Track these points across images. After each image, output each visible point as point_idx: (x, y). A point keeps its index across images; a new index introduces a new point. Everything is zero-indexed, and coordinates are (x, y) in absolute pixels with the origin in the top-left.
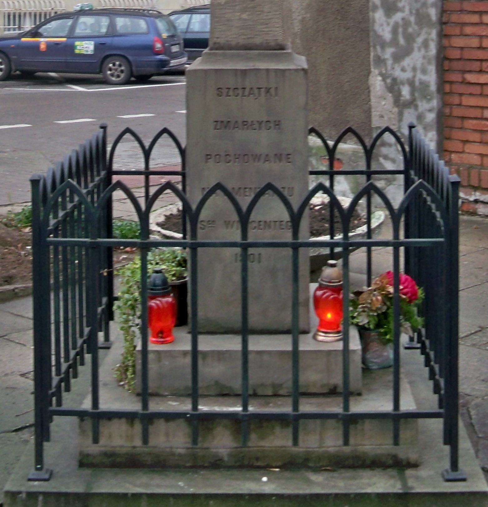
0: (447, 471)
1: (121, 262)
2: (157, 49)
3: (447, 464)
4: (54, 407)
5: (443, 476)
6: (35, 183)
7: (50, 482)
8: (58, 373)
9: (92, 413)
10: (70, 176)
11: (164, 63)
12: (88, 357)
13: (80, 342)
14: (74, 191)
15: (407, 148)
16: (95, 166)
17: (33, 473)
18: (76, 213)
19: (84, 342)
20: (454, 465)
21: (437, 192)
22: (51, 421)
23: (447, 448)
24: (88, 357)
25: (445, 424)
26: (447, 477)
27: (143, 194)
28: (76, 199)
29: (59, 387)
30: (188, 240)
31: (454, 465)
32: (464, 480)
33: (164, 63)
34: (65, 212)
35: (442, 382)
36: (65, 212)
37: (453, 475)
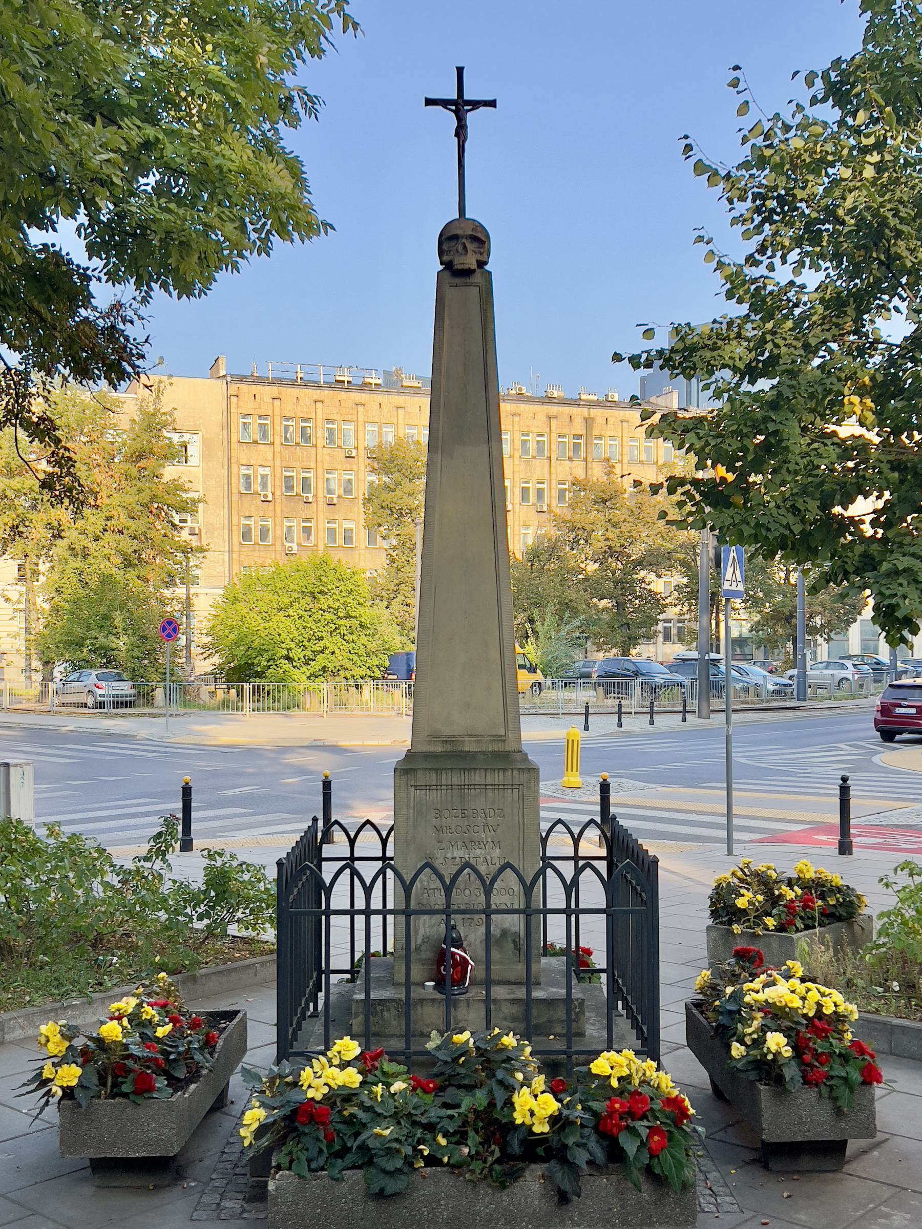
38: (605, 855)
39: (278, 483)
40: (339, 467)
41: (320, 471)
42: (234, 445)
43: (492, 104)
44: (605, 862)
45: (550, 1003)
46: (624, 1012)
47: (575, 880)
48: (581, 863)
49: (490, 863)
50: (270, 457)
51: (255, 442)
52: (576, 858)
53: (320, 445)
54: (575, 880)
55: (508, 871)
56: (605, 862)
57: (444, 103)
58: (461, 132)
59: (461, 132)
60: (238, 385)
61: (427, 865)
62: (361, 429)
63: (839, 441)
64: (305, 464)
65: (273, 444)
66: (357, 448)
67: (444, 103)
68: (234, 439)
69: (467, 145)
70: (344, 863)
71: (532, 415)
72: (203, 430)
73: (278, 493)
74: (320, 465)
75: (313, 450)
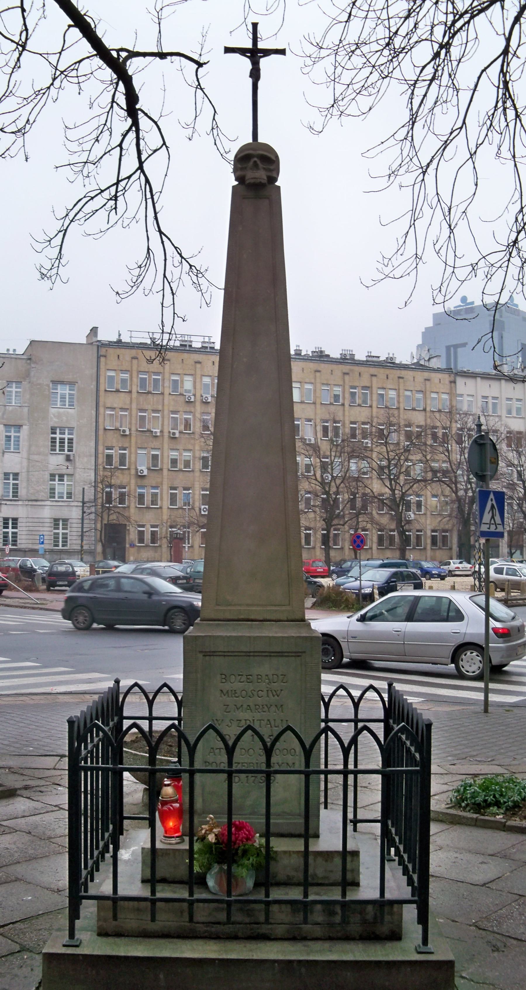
2: (83, 774)
3: (420, 941)
4: (83, 894)
6: (71, 722)
7: (80, 948)
8: (86, 867)
9: (113, 898)
11: (187, 541)
14: (99, 728)
15: (386, 696)
16: (105, 709)
18: (180, 582)
21: (412, 728)
22: (81, 904)
23: (420, 927)
25: (418, 908)
26: (419, 950)
28: (101, 734)
29: (86, 879)
30: (186, 765)
33: (187, 541)
34: (93, 744)
35: (415, 877)
36: (93, 744)
37: (423, 949)
38: (124, 720)
39: (134, 421)
40: (181, 409)
41: (166, 412)
42: (102, 393)
43: (282, 52)
44: (382, 724)
45: (328, 855)
46: (397, 858)
47: (354, 741)
48: (360, 725)
49: (273, 725)
50: (128, 402)
51: (118, 391)
52: (356, 721)
53: (167, 392)
54: (354, 741)
55: (289, 733)
56: (382, 724)
57: (242, 51)
58: (255, 74)
59: (255, 74)
60: (107, 349)
61: (211, 727)
62: (198, 380)
63: (477, 580)
64: (155, 407)
65: (130, 392)
66: (195, 395)
67: (242, 51)
68: (102, 388)
69: (260, 84)
70: (170, 722)
71: (330, 371)
72: (79, 382)
73: (133, 429)
74: (166, 408)
75: (161, 397)
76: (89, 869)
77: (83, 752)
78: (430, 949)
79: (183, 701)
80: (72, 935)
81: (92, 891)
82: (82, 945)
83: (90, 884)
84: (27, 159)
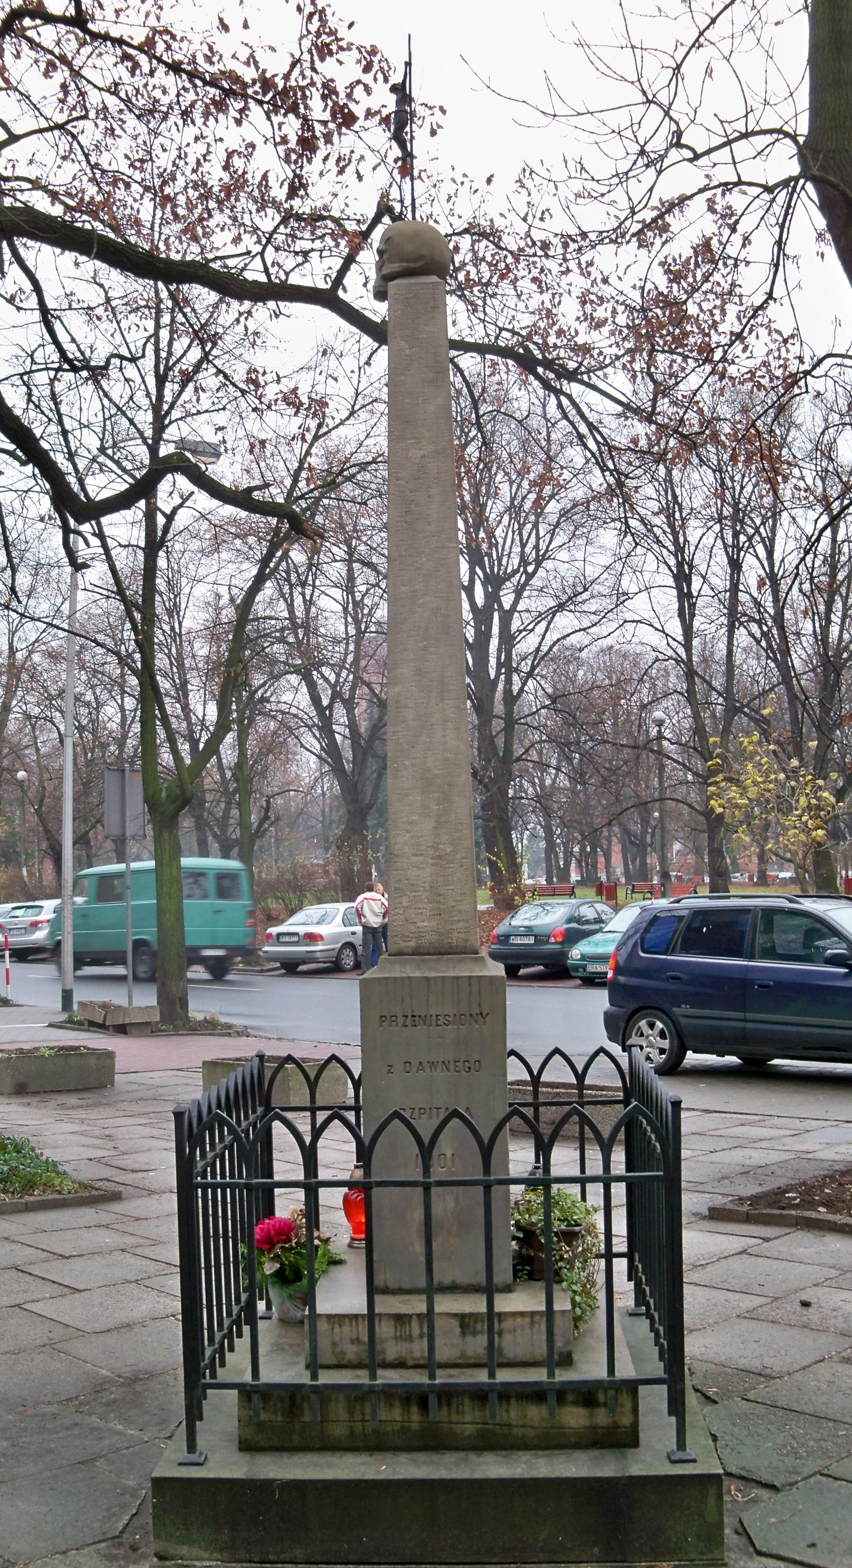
0: (673, 1452)
1: (355, 785)
3: (673, 1444)
4: (208, 1380)
5: (668, 1457)
6: (178, 1116)
10: (219, 1106)
12: (246, 1329)
13: (235, 1309)
16: (240, 1088)
17: (185, 1456)
19: (241, 1310)
20: (681, 1444)
24: (246, 1329)
26: (673, 1458)
27: (309, 1127)
31: (681, 1444)
32: (694, 1461)
37: (679, 1455)
76: (217, 1346)
77: (200, 1165)
78: (689, 1455)
79: (363, 1082)
80: (192, 1447)
81: (223, 1375)
82: (207, 1466)
83: (228, 1355)
84: (273, 49)
